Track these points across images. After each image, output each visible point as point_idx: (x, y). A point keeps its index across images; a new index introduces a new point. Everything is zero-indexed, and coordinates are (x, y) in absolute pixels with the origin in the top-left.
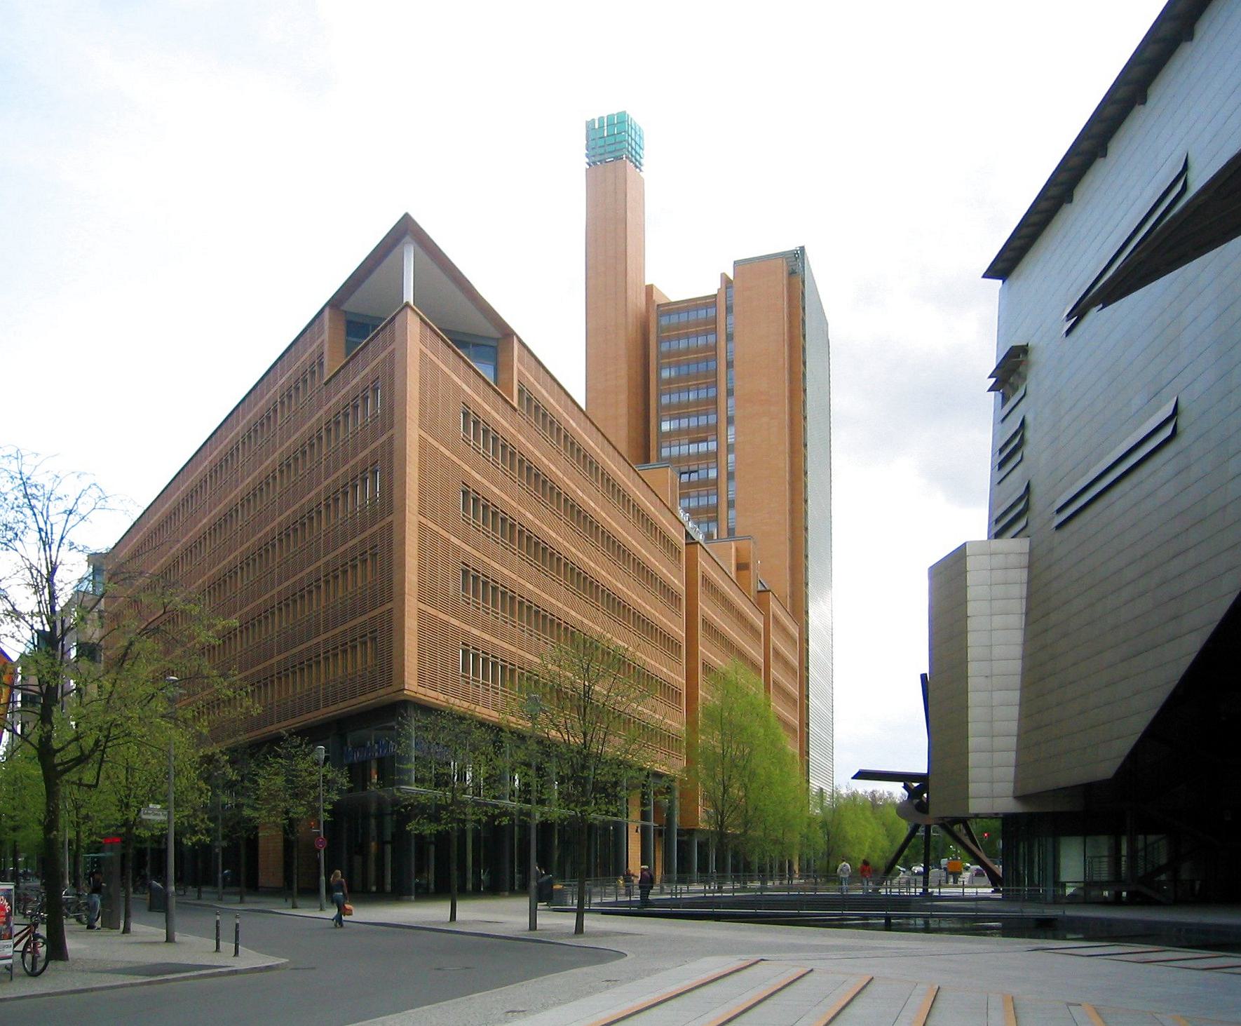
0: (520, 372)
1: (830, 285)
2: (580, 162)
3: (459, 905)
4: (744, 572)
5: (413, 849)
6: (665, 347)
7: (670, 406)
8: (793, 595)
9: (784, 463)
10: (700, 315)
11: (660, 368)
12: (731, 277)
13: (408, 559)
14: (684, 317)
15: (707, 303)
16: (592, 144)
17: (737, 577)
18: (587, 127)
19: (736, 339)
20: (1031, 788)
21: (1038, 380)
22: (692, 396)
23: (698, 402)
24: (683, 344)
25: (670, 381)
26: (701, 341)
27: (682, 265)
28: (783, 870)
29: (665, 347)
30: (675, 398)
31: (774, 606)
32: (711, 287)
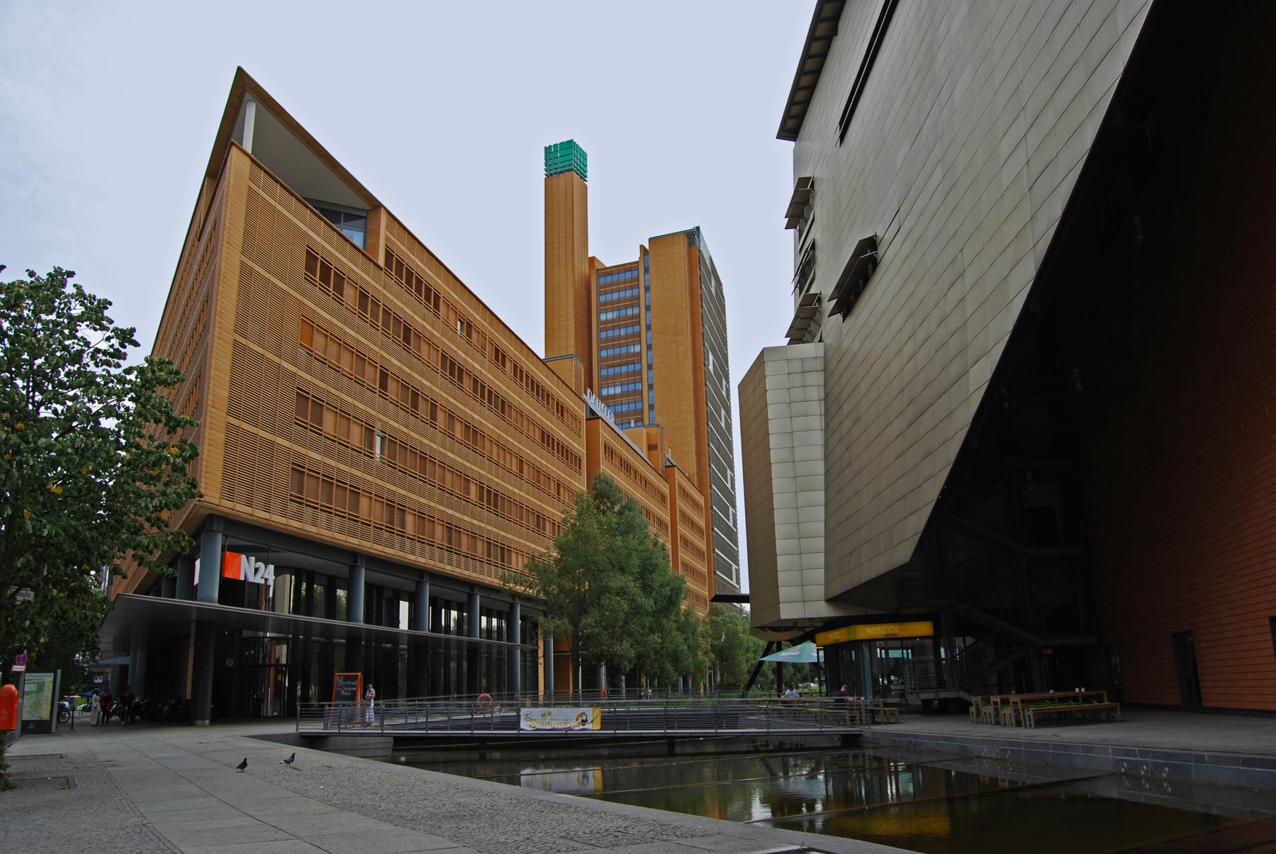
0: (387, 239)
1: (712, 246)
4: (654, 452)
6: (602, 298)
7: (605, 304)
8: (699, 474)
11: (599, 313)
14: (615, 278)
17: (649, 457)
20: (838, 590)
21: (821, 209)
22: (623, 332)
23: (626, 337)
24: (616, 296)
25: (606, 322)
26: (629, 293)
27: (613, 241)
28: (689, 680)
29: (602, 298)
31: (678, 477)
32: (635, 256)
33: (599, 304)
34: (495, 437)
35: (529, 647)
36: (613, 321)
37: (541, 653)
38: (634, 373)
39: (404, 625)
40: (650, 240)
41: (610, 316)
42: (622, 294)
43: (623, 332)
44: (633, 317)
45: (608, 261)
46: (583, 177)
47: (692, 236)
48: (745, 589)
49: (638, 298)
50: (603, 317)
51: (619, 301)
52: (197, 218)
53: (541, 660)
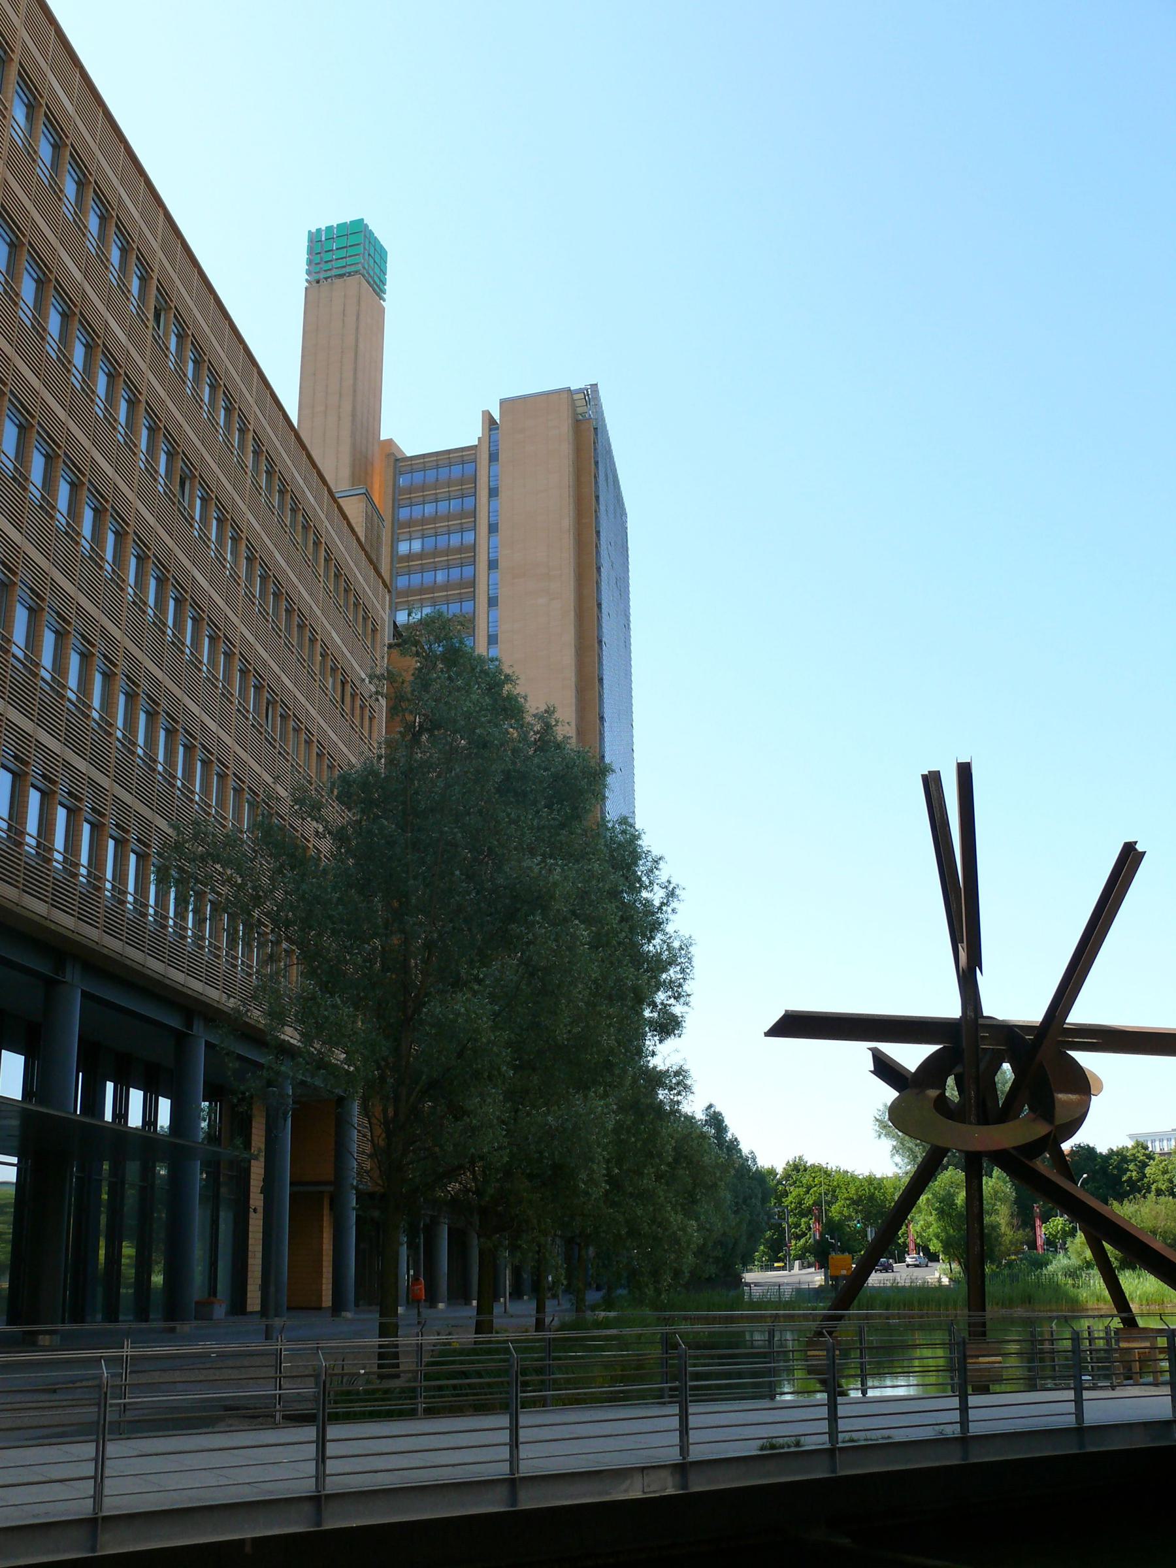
2: (303, 256)
9: (567, 658)
16: (317, 259)
19: (504, 494)
22: (441, 577)
23: (446, 587)
25: (409, 557)
27: (428, 407)
30: (416, 579)
32: (469, 434)
33: (397, 524)
35: (667, 1393)
37: (257, 1171)
39: (108, 1117)
40: (503, 403)
42: (443, 506)
43: (441, 577)
44: (461, 549)
45: (411, 447)
46: (378, 289)
47: (590, 395)
48: (871, 1393)
50: (403, 548)
51: (435, 519)
53: (256, 1199)
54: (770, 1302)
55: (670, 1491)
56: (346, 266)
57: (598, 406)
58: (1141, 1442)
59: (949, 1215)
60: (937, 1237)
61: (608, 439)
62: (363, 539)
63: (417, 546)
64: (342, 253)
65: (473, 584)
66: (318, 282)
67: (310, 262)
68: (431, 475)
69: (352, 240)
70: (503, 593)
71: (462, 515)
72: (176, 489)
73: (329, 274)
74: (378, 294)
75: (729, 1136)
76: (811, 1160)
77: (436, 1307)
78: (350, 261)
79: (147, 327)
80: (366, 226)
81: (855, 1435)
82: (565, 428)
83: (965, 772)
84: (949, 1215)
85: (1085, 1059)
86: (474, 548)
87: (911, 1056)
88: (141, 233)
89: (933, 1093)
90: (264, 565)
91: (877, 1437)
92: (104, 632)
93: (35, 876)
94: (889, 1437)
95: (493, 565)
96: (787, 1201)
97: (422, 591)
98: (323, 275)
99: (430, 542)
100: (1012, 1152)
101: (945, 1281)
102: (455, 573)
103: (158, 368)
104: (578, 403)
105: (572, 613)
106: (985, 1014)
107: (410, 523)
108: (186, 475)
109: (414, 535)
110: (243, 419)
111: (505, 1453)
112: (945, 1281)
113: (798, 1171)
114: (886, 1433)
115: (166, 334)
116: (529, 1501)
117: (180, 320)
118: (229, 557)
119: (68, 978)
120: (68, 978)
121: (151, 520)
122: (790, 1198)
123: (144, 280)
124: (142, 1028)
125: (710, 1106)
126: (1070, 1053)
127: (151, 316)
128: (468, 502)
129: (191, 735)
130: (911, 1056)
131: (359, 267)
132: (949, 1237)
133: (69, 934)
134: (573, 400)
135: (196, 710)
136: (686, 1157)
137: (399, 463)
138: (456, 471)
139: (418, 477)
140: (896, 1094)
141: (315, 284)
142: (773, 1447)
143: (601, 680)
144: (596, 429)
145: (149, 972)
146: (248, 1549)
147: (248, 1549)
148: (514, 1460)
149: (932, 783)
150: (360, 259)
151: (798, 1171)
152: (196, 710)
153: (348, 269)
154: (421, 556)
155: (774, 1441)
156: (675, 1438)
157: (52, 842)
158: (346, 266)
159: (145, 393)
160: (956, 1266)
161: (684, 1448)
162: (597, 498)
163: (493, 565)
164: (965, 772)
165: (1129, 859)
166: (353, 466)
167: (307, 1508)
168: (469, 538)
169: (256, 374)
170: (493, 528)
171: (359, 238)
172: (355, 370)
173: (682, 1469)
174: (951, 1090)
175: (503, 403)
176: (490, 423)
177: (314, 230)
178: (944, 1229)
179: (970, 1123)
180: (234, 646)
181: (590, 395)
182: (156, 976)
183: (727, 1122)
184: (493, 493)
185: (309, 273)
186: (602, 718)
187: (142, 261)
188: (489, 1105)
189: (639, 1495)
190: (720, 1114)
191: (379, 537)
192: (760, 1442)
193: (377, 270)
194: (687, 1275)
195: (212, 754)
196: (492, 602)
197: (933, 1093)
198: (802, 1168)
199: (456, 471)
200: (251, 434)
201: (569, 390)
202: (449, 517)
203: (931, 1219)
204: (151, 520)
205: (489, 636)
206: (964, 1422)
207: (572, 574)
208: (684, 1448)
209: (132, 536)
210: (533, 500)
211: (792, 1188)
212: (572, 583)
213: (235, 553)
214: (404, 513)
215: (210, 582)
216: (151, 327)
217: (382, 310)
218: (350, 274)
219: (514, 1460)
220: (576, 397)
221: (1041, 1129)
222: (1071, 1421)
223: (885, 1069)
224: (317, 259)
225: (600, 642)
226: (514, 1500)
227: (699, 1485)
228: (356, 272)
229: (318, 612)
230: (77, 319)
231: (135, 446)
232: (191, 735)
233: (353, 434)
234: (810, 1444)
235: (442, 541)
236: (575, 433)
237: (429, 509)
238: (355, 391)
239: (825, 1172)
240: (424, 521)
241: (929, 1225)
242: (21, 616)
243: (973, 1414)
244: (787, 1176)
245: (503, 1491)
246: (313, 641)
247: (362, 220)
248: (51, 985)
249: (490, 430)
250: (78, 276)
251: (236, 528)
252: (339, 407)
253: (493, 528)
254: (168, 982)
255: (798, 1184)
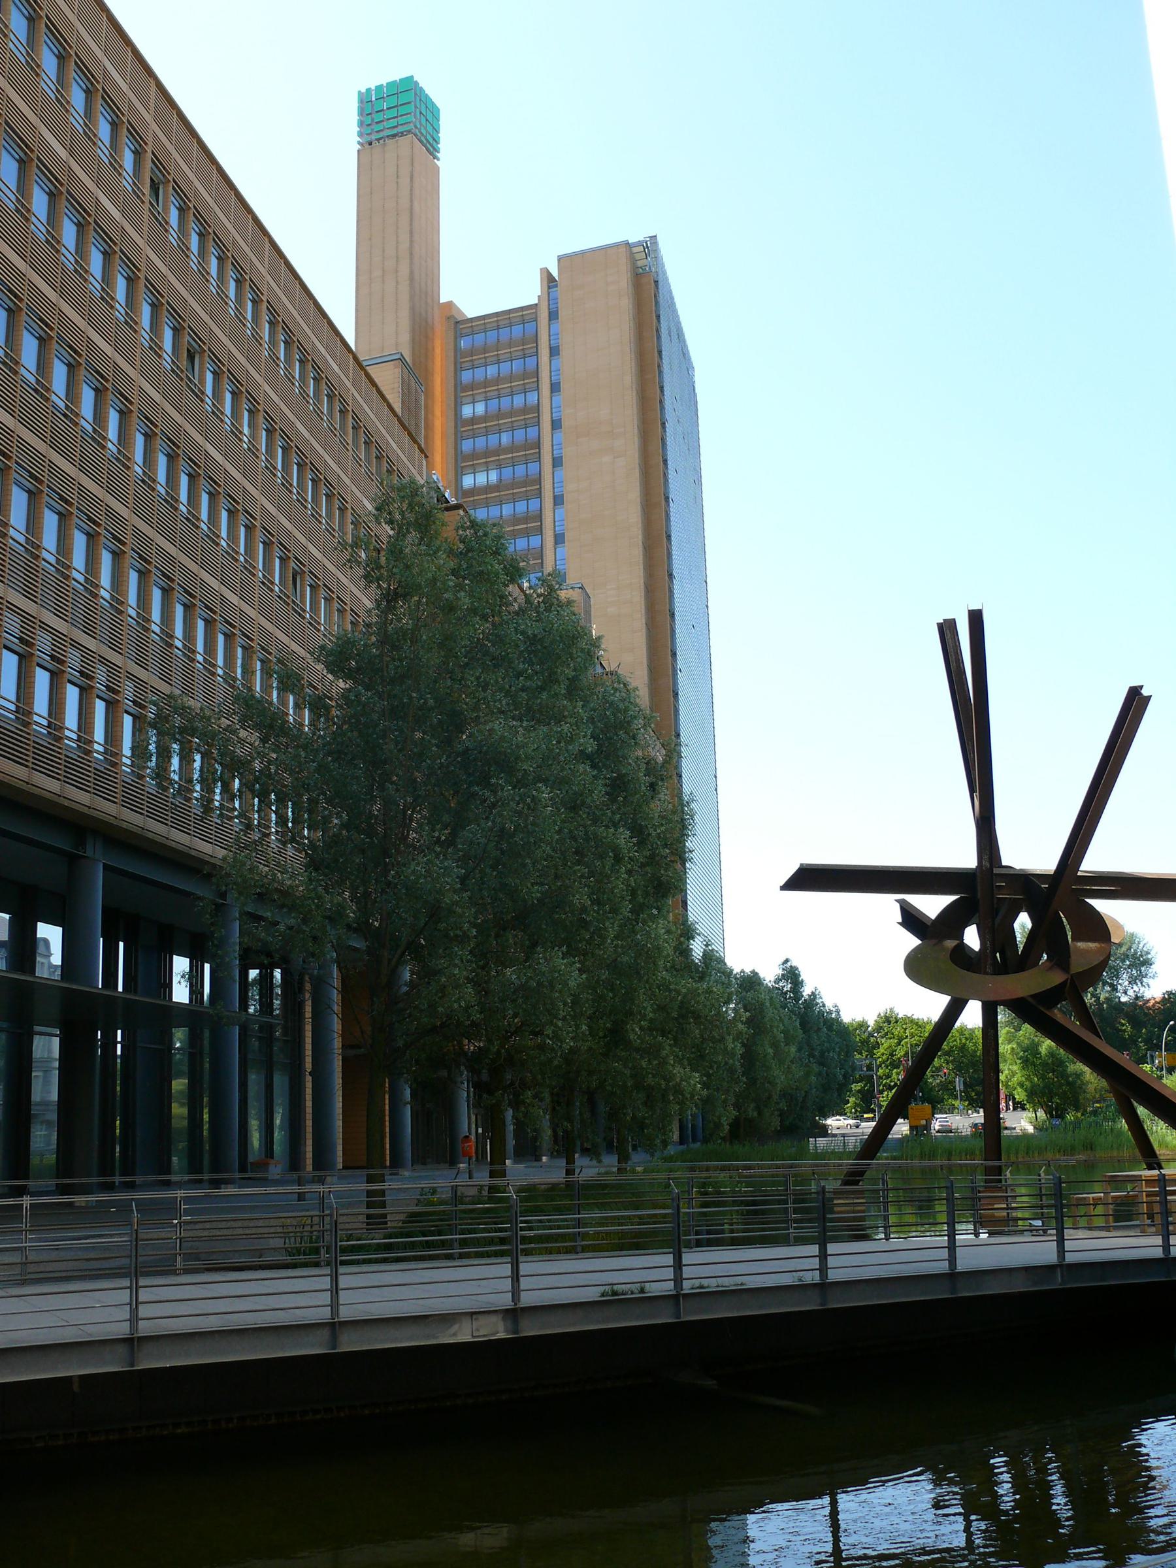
2: (354, 118)
3: (842, 1498)
5: (567, 1281)
7: (474, 455)
9: (633, 516)
10: (511, 337)
12: (555, 273)
13: (340, 1069)
14: (492, 336)
15: (522, 316)
16: (368, 120)
18: (361, 101)
19: (565, 352)
22: (505, 438)
23: (512, 449)
25: (473, 420)
27: (485, 271)
30: (480, 443)
32: (528, 293)
34: (295, 551)
36: (488, 488)
38: (527, 445)
40: (561, 259)
41: (481, 479)
42: (505, 368)
43: (505, 438)
44: (525, 410)
45: (471, 308)
46: (431, 147)
47: (650, 247)
49: (540, 517)
50: (467, 411)
51: (498, 380)
52: (39, 1292)
54: (833, 1152)
55: (502, 1335)
56: (398, 127)
57: (657, 258)
58: (1020, 1286)
59: (1033, 1064)
60: (1021, 1085)
61: (670, 292)
62: (398, 407)
63: (480, 408)
64: (393, 113)
65: (538, 445)
66: (370, 144)
67: (361, 124)
68: (492, 336)
69: (403, 99)
70: (568, 453)
71: (525, 375)
72: (184, 363)
73: (380, 135)
74: (431, 154)
75: (807, 991)
76: (902, 1012)
77: (540, 1160)
78: (401, 120)
79: (143, 202)
80: (416, 83)
81: (705, 1282)
82: (623, 281)
83: (976, 618)
84: (1033, 1064)
85: (1100, 905)
86: (537, 408)
87: (932, 905)
88: (131, 105)
89: (950, 944)
90: (285, 436)
91: (729, 1283)
92: (110, 512)
93: (47, 751)
94: (742, 1284)
95: (556, 425)
96: (879, 1052)
97: (487, 453)
98: (373, 137)
99: (493, 404)
100: (1030, 1000)
101: (1030, 1129)
102: (520, 435)
103: (158, 242)
104: (638, 257)
105: (637, 470)
106: (1004, 863)
107: (472, 387)
108: (193, 352)
109: (477, 398)
110: (255, 289)
111: (326, 1298)
112: (1030, 1129)
113: (889, 1023)
114: (739, 1280)
115: (166, 209)
116: (350, 1343)
117: (178, 191)
118: (246, 430)
119: (89, 853)
120: (89, 853)
121: (157, 397)
122: (882, 1050)
123: (138, 154)
124: (158, 900)
125: (787, 961)
126: (1088, 900)
127: (147, 190)
128: (531, 362)
129: (211, 610)
130: (932, 905)
131: (411, 126)
132: (1033, 1086)
133: (85, 810)
134: (632, 254)
135: (214, 584)
136: (693, 1012)
137: (460, 326)
138: (517, 330)
139: (479, 339)
140: (920, 942)
141: (367, 146)
142: (615, 1293)
143: (669, 537)
144: (656, 282)
145: (173, 845)
146: (76, 1387)
147: (76, 1387)
148: (334, 1305)
149: (947, 630)
150: (410, 118)
151: (889, 1023)
152: (214, 584)
153: (400, 129)
154: (485, 418)
155: (615, 1287)
156: (507, 1284)
157: (63, 720)
158: (398, 127)
159: (143, 269)
160: (1041, 1114)
161: (516, 1293)
162: (660, 352)
163: (556, 425)
164: (976, 618)
165: (1135, 705)
166: (413, 331)
167: (122, 1350)
168: (532, 398)
169: (267, 244)
170: (555, 388)
171: (410, 97)
172: (411, 232)
173: (513, 1314)
174: (972, 937)
175: (561, 259)
176: (549, 281)
177: (363, 91)
178: (1028, 1078)
179: (987, 974)
180: (255, 519)
181: (650, 247)
182: (180, 848)
183: (803, 976)
184: (554, 351)
185: (361, 135)
186: (671, 576)
187: (134, 133)
188: (458, 966)
189: (467, 1338)
190: (797, 969)
191: (417, 402)
192: (602, 1289)
193: (429, 128)
194: (727, 1128)
195: (234, 627)
196: (557, 462)
197: (950, 944)
198: (893, 1020)
199: (517, 330)
200: (265, 304)
201: (627, 243)
202: (511, 378)
203: (1015, 1068)
204: (157, 397)
205: (555, 497)
206: (823, 1269)
207: (636, 431)
208: (516, 1293)
209: (135, 414)
210: (594, 355)
211: (883, 1040)
212: (636, 439)
213: (252, 425)
214: (466, 376)
215: (225, 456)
216: (147, 201)
217: (437, 170)
218: (402, 134)
219: (334, 1305)
220: (635, 250)
221: (1057, 978)
222: (943, 1267)
223: (911, 920)
224: (368, 120)
225: (667, 498)
226: (334, 1342)
227: (531, 1329)
228: (409, 132)
229: (347, 481)
230: (64, 197)
231: (136, 323)
232: (211, 610)
233: (412, 298)
234: (655, 1289)
235: (505, 402)
236: (638, 283)
237: (492, 371)
238: (411, 254)
239: (917, 1024)
240: (486, 383)
241: (1014, 1074)
242: (18, 501)
243: (831, 1262)
244: (879, 1028)
245: (325, 1333)
246: (342, 510)
247: (412, 77)
248: (73, 860)
249: (549, 288)
250: (63, 153)
251: (253, 399)
252: (397, 271)
253: (555, 388)
254: (193, 853)
255: (889, 1035)
